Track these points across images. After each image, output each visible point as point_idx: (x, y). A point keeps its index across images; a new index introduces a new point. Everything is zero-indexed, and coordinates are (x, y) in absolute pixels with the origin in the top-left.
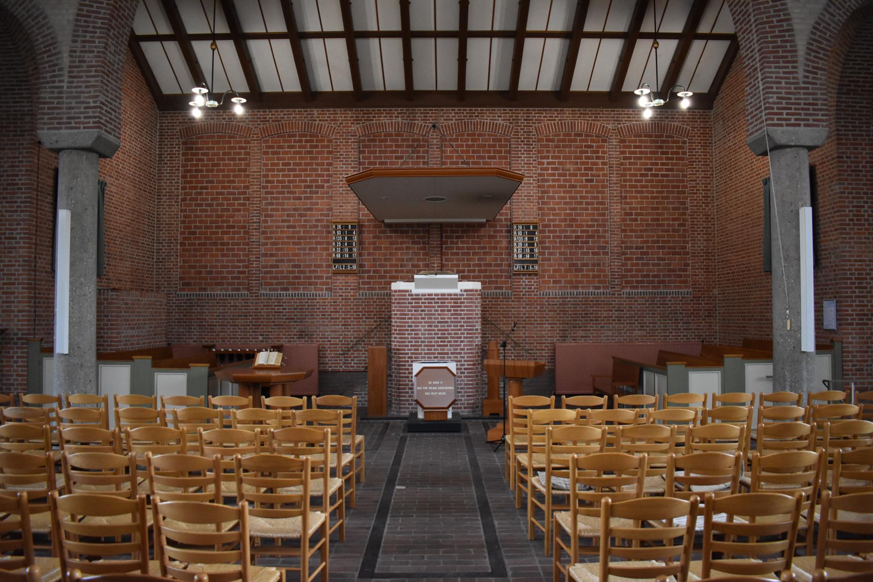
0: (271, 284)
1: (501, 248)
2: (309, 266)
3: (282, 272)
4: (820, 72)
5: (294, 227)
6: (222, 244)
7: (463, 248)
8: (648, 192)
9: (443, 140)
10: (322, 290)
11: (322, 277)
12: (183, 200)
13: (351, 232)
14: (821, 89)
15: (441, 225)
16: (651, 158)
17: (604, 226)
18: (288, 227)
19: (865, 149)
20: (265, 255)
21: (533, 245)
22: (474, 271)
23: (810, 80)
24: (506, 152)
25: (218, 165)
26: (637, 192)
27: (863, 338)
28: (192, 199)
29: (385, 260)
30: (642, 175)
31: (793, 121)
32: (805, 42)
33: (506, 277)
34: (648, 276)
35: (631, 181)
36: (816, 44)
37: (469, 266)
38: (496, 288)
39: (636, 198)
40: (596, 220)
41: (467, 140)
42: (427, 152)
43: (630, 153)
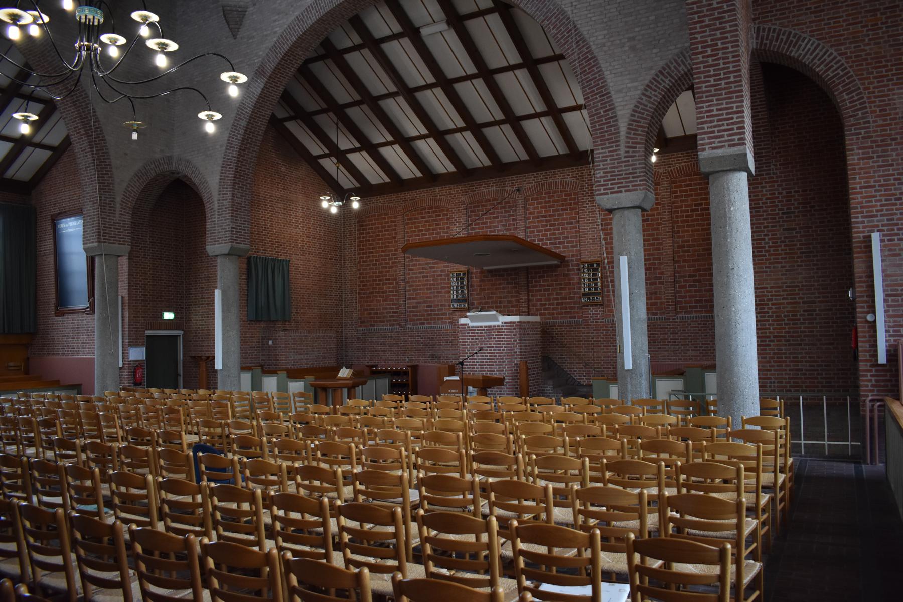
0: (414, 320)
1: (574, 284)
3: (420, 311)
6: (383, 292)
7: (544, 286)
8: (699, 225)
9: (526, 199)
11: (446, 314)
12: (359, 262)
13: (462, 279)
15: (527, 268)
16: (701, 194)
17: (659, 259)
18: (423, 277)
19: (765, 187)
20: (409, 299)
21: (597, 279)
22: (553, 304)
23: (631, 154)
26: (688, 226)
27: (765, 358)
28: (364, 262)
29: (489, 298)
30: (692, 210)
31: (616, 189)
32: (626, 124)
33: (578, 308)
34: (701, 301)
35: (682, 216)
37: (549, 300)
38: (570, 317)
39: (688, 231)
40: (652, 255)
43: (681, 191)
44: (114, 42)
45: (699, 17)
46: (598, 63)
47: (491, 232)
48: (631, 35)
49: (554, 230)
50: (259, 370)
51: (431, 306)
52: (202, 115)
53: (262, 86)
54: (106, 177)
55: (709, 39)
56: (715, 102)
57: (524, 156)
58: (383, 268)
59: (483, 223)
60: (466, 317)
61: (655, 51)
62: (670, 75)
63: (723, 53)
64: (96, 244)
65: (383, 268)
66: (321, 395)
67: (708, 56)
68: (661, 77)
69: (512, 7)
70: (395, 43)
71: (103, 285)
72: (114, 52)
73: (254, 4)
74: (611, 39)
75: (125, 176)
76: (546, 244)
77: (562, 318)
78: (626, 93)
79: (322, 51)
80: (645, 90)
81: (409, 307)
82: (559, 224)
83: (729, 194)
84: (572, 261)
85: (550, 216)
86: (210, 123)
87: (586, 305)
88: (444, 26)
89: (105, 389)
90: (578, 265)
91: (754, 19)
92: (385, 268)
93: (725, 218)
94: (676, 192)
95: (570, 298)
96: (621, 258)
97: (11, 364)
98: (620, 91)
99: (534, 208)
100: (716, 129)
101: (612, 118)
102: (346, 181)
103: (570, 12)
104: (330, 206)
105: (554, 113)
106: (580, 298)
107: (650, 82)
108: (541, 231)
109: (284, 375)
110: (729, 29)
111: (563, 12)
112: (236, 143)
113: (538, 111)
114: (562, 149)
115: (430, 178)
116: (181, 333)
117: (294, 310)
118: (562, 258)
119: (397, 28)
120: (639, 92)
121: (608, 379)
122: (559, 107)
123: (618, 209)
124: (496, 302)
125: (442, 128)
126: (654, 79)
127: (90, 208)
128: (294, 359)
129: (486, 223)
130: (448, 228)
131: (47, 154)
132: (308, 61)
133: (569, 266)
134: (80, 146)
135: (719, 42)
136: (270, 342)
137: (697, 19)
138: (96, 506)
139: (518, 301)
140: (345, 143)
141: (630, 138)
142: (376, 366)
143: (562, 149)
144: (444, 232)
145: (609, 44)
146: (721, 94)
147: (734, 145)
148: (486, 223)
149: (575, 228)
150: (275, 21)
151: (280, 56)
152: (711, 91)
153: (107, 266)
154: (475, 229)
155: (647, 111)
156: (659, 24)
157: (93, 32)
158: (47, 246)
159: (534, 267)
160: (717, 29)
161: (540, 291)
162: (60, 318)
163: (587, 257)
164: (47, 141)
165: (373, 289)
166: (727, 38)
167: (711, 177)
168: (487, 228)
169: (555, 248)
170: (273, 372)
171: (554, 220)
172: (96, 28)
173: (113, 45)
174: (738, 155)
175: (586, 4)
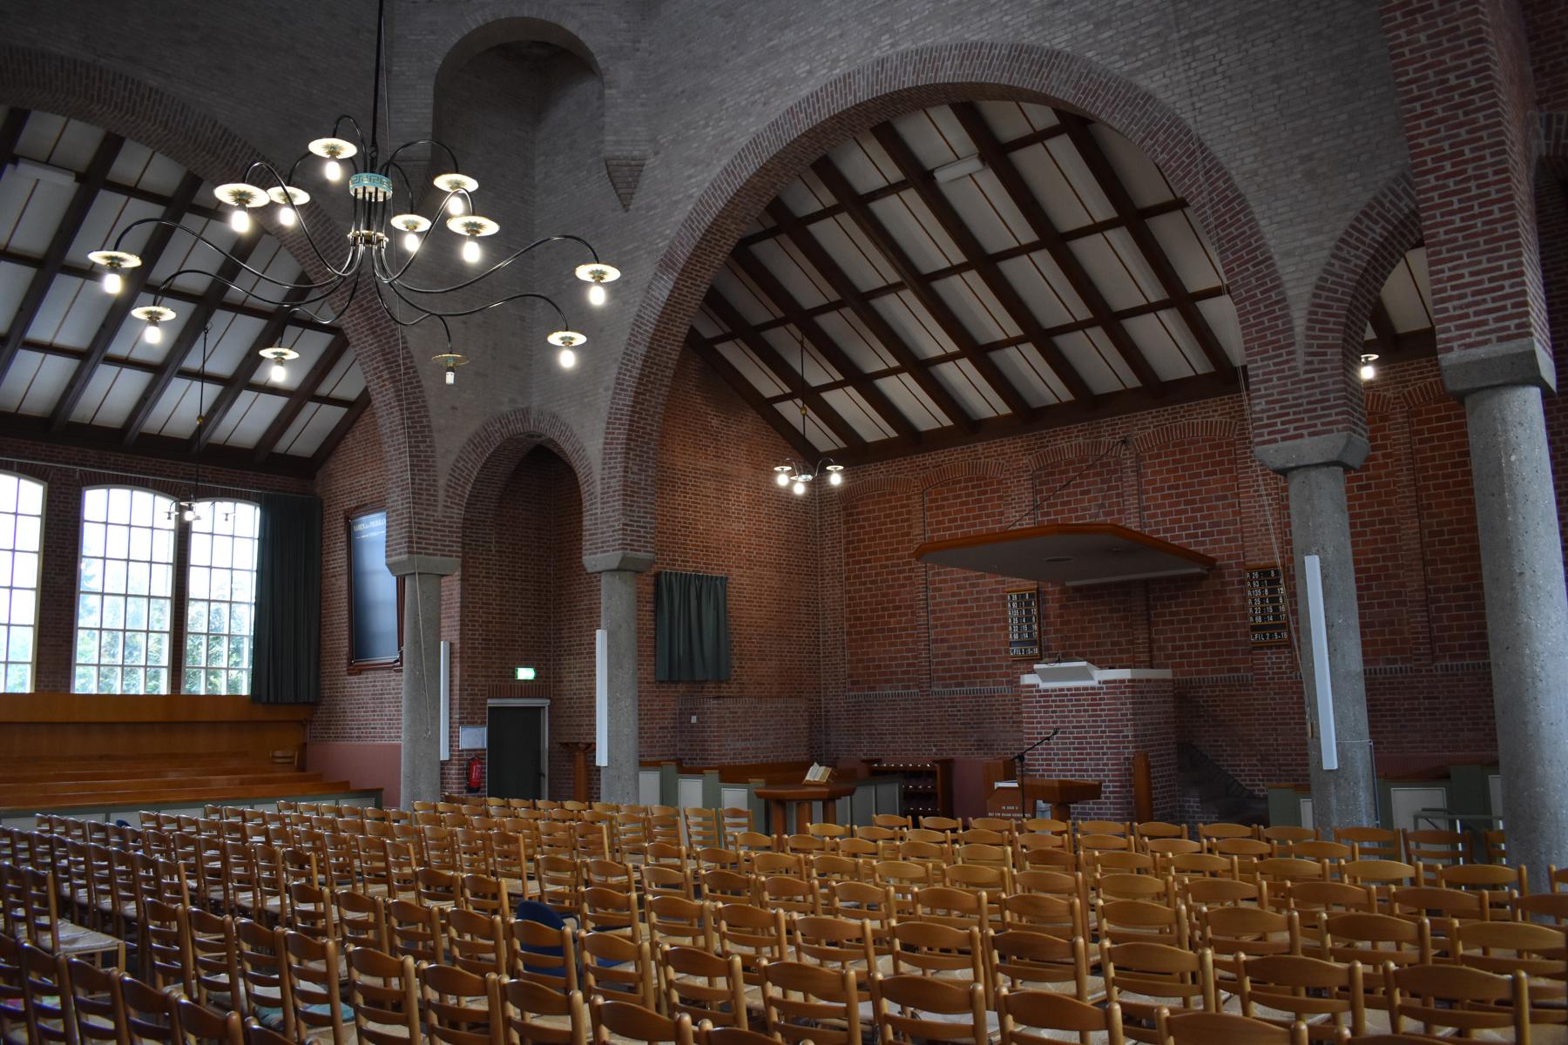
2: (986, 652)
3: (955, 662)
4: (1329, 351)
5: (966, 601)
7: (1178, 613)
10: (1002, 683)
11: (1000, 667)
12: (847, 578)
13: (1028, 604)
14: (1331, 376)
15: (1146, 582)
18: (960, 602)
20: (936, 641)
22: (1196, 646)
23: (1316, 366)
24: (1230, 462)
25: (880, 531)
28: (856, 577)
29: (1077, 638)
31: (1292, 432)
35: (1435, 477)
36: (1321, 310)
37: (1189, 638)
38: (1230, 670)
40: (1382, 550)
41: (1174, 453)
42: (1120, 479)
43: (1431, 430)
44: (412, 227)
45: (1423, 106)
46: (1248, 206)
47: (1077, 518)
48: (1305, 151)
49: (1193, 510)
50: (673, 767)
51: (973, 653)
52: (555, 339)
53: (670, 285)
54: (422, 447)
55: (1446, 144)
56: (1466, 260)
57: (1133, 381)
58: (889, 587)
59: (1063, 504)
60: (1033, 672)
61: (1350, 176)
62: (1383, 217)
63: (1475, 169)
64: (405, 557)
65: (889, 587)
66: (777, 813)
67: (1447, 176)
68: (1366, 221)
69: (1092, 122)
70: (893, 200)
71: (416, 622)
72: (412, 244)
73: (657, 153)
74: (1269, 162)
75: (453, 444)
76: (1180, 537)
77: (1213, 671)
78: (1301, 258)
79: (770, 223)
80: (1339, 248)
81: (936, 656)
82: (1201, 501)
83: (1506, 431)
84: (1230, 566)
85: (1185, 486)
86: (567, 351)
87: (1259, 647)
88: (974, 165)
89: (415, 798)
90: (1240, 574)
91: (1539, 103)
92: (892, 587)
93: (1500, 476)
94: (1420, 432)
95: (1228, 635)
96: (1307, 559)
97: (278, 753)
98: (1288, 254)
99: (1153, 473)
100: (1471, 310)
101: (1277, 302)
102: (820, 436)
103: (1190, 121)
104: (792, 482)
105: (1182, 301)
106: (1247, 635)
107: (1347, 232)
108: (1170, 513)
109: (713, 776)
110: (1482, 122)
111: (1177, 121)
112: (630, 382)
113: (1153, 299)
114: (1202, 366)
115: (966, 427)
116: (545, 702)
117: (735, 663)
118: (1209, 562)
119: (895, 174)
120: (1326, 253)
121: (1297, 787)
122: (1191, 290)
123: (1297, 468)
124: (1091, 645)
125: (983, 340)
126: (1353, 227)
127: (398, 498)
128: (732, 748)
129: (1068, 503)
130: (1001, 514)
131: (341, 411)
132: (745, 243)
133: (1223, 576)
134: (383, 399)
135: (1466, 149)
136: (694, 719)
137: (1419, 111)
138: (328, 1006)
139: (1131, 642)
140: (816, 373)
141: (1314, 338)
142: (879, 761)
143: (1202, 366)
144: (995, 522)
145: (1266, 170)
146: (1477, 244)
147: (1509, 338)
148: (1068, 503)
149: (1233, 505)
150: (690, 177)
151: (698, 235)
152: (1456, 240)
153: (423, 592)
154: (1048, 514)
155: (1344, 286)
156: (1358, 128)
157: (374, 213)
158: (338, 560)
159: (1159, 580)
160: (1461, 125)
161: (1172, 622)
162: (354, 679)
163: (1255, 558)
164: (339, 393)
165: (873, 624)
166: (1481, 138)
167: (1468, 401)
168: (1070, 511)
169: (1196, 544)
170: (695, 772)
171: (1193, 493)
172: (380, 209)
173: (411, 231)
174: (1517, 355)
175: (1220, 105)
